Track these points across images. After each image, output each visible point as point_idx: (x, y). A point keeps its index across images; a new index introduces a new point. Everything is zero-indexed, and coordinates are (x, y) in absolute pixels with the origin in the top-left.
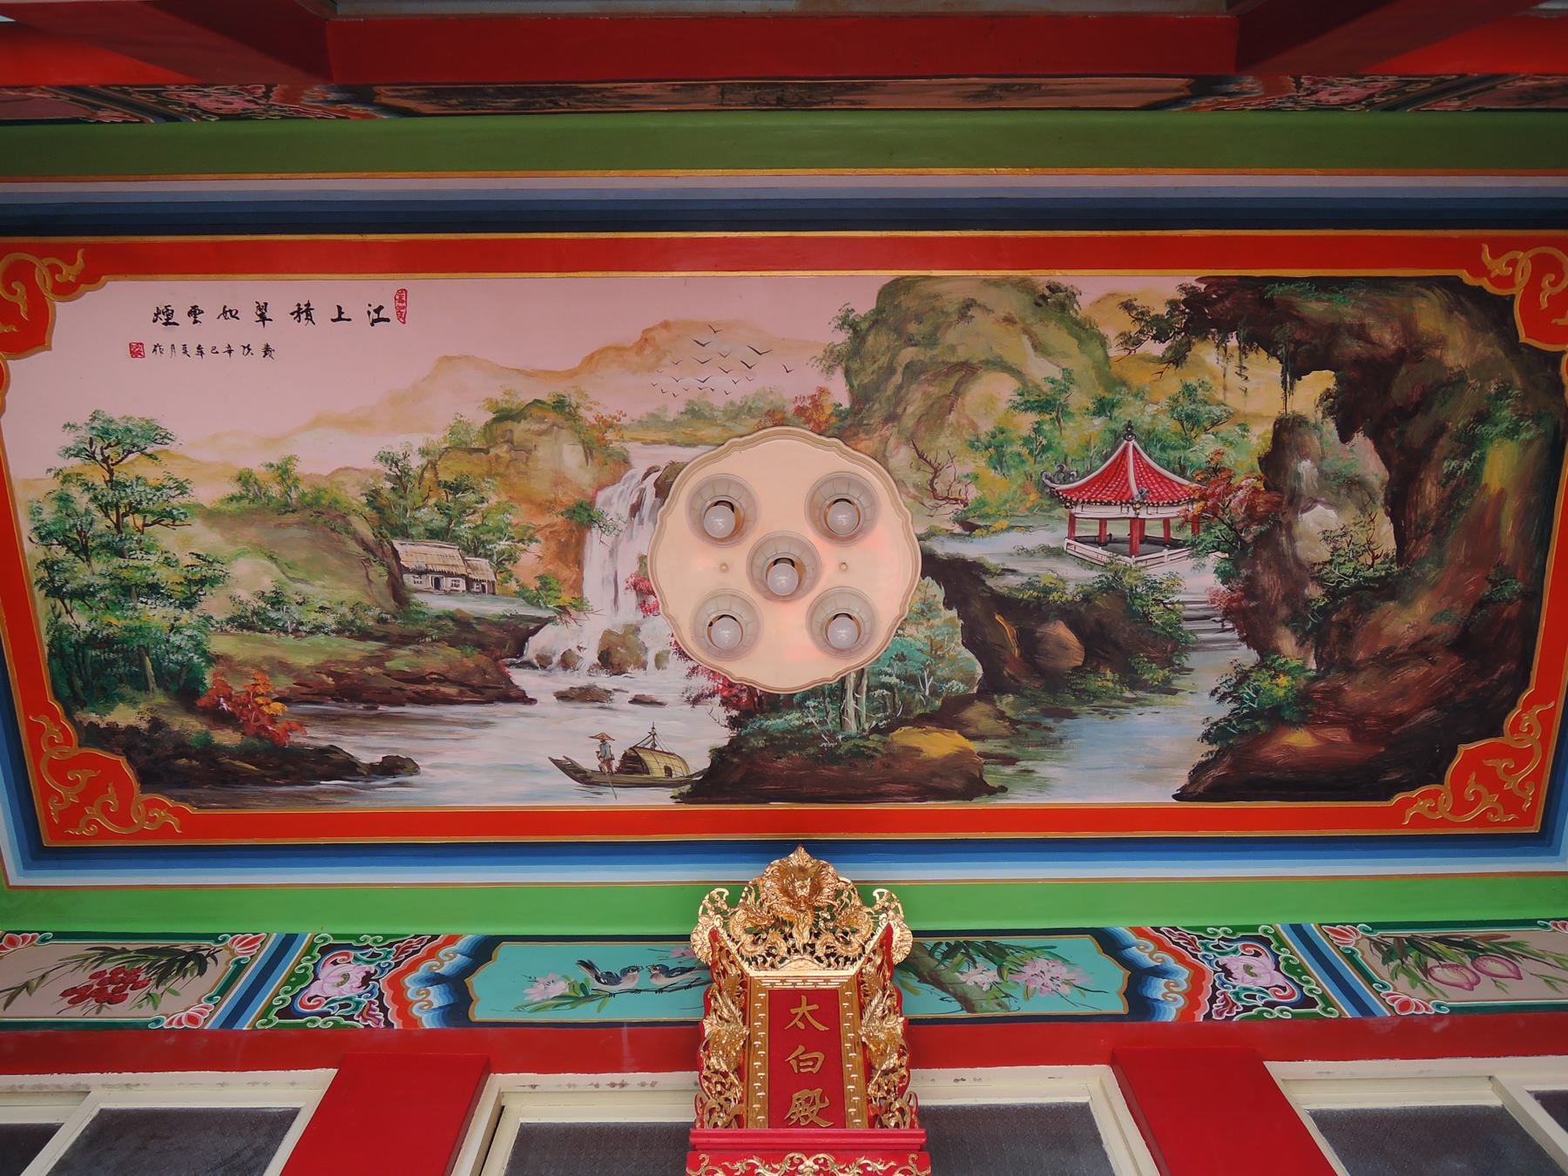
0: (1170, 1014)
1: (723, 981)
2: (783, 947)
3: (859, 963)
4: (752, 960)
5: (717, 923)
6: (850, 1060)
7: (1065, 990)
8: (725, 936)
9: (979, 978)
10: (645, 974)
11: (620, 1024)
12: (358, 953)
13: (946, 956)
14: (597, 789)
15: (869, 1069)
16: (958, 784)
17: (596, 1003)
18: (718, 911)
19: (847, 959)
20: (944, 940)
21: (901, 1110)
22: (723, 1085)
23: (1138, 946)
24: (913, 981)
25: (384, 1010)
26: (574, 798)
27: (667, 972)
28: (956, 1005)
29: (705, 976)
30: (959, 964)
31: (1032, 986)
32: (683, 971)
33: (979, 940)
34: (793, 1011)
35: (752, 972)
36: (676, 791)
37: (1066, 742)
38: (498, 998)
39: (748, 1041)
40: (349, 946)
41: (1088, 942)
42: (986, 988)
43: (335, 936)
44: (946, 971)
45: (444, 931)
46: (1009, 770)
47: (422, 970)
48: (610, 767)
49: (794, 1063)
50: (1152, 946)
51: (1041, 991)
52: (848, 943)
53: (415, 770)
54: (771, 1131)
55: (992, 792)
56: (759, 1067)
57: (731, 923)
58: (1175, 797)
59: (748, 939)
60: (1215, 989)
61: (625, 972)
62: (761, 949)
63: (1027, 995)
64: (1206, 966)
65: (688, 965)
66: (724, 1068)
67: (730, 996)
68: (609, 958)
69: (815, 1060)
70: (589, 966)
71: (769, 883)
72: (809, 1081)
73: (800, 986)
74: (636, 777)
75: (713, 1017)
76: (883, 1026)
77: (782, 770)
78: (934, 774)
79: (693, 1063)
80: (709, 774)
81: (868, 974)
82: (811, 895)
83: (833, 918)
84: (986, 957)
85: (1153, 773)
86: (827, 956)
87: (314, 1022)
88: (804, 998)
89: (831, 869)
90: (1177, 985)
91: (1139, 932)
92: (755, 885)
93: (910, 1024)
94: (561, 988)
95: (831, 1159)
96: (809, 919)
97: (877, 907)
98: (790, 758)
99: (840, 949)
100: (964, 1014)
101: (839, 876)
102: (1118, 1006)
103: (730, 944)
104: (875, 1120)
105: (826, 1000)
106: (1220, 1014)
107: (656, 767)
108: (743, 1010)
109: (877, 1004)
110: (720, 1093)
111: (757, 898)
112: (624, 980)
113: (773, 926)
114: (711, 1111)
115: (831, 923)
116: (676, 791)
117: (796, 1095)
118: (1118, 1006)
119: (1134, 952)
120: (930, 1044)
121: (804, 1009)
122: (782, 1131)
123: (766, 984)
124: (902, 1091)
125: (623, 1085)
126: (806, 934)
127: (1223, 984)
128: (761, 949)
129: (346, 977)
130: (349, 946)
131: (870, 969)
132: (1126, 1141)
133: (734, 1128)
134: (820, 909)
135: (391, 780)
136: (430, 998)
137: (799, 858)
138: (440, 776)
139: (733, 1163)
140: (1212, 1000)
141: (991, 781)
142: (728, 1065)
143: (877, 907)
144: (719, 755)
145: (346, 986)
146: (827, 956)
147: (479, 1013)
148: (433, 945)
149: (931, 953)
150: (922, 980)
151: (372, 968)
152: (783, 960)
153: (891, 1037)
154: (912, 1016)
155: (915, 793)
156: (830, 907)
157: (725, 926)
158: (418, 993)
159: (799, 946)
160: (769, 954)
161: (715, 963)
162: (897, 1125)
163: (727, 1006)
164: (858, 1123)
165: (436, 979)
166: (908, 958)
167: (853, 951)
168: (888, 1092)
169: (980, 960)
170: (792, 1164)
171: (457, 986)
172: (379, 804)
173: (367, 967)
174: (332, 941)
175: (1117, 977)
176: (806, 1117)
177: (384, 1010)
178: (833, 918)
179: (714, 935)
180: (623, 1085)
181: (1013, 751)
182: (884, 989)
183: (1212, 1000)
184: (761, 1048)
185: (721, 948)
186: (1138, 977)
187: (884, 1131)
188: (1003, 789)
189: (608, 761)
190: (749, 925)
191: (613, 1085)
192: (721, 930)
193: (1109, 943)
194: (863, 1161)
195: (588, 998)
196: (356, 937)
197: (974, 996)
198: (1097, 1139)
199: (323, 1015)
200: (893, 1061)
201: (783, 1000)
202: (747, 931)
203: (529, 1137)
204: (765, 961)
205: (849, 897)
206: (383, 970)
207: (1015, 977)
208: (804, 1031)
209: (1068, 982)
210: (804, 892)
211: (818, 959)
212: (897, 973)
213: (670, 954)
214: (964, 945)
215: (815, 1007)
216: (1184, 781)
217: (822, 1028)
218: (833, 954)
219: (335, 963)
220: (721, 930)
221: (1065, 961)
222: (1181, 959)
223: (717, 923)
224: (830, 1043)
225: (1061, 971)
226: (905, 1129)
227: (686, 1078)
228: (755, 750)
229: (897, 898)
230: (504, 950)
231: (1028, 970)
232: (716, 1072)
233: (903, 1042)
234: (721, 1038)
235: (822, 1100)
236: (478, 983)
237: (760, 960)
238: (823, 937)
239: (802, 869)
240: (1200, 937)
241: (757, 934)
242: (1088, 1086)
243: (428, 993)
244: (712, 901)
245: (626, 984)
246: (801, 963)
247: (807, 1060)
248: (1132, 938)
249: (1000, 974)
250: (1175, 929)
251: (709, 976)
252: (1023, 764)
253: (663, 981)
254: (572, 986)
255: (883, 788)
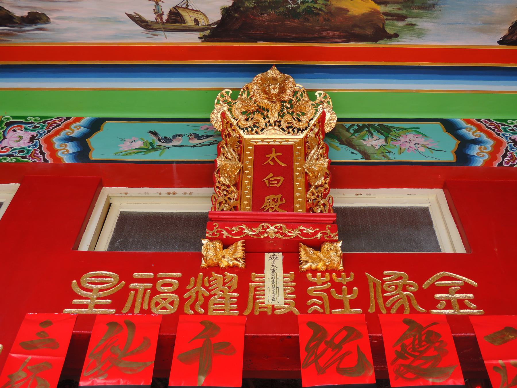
0: (479, 163)
1: (228, 139)
2: (263, 123)
3: (306, 132)
4: (245, 129)
5: (225, 109)
6: (298, 181)
7: (422, 150)
8: (230, 116)
9: (374, 143)
10: (186, 138)
11: (172, 162)
12: (27, 126)
13: (356, 131)
14: (155, 33)
15: (308, 186)
16: (369, 32)
17: (158, 152)
18: (225, 102)
19: (299, 130)
20: (356, 123)
21: (324, 205)
22: (227, 191)
23: (466, 129)
24: (336, 143)
25: (43, 154)
26: (141, 38)
27: (198, 137)
28: (360, 156)
29: (219, 139)
30: (363, 136)
31: (403, 147)
32: (207, 137)
33: (376, 124)
34: (267, 156)
35: (245, 136)
36: (201, 34)
37: (436, 7)
38: (104, 148)
39: (242, 171)
40: (22, 123)
41: (438, 126)
42: (377, 148)
43: (14, 117)
44: (356, 139)
45: (74, 115)
46: (401, 24)
47: (63, 134)
48: (161, 19)
49: (267, 182)
50: (474, 129)
51: (408, 150)
52: (300, 121)
53: (47, 20)
54: (253, 213)
55: (390, 37)
56: (247, 183)
57: (233, 109)
58: (499, 42)
59: (242, 118)
60: (507, 151)
61: (174, 137)
62: (250, 123)
63: (400, 152)
64: (504, 139)
65: (209, 134)
66: (228, 183)
67: (232, 147)
68: (165, 130)
69: (279, 181)
70: (155, 134)
71: (255, 87)
72: (275, 191)
73: (272, 143)
74: (177, 26)
75: (222, 158)
76: (318, 163)
77: (264, 21)
78: (355, 26)
79: (210, 182)
80: (221, 24)
81: (311, 137)
82: (279, 93)
83: (292, 107)
84: (379, 132)
85: (487, 27)
86: (288, 128)
87: (5, 159)
88: (274, 150)
89: (291, 80)
90: (486, 149)
91: (468, 121)
92: (247, 88)
93: (331, 164)
94: (139, 144)
95: (284, 227)
96: (278, 107)
97: (317, 101)
98: (269, 14)
99: (295, 124)
100: (364, 160)
101: (296, 85)
102: (451, 158)
103: (233, 120)
104: (310, 209)
105: (286, 151)
106: (508, 163)
107: (189, 19)
108: (239, 155)
109: (315, 152)
110: (225, 195)
111: (248, 95)
112: (174, 140)
113: (257, 111)
114: (220, 203)
115: (290, 108)
116: (201, 34)
117: (267, 198)
118: (451, 158)
119: (464, 131)
120: (341, 175)
121: (274, 155)
122: (258, 213)
123: (253, 142)
124: (325, 196)
125: (174, 194)
126: (276, 115)
127: (512, 148)
128: (250, 123)
129: (21, 138)
130: (22, 123)
131: (312, 134)
132: (440, 207)
133: (233, 211)
134: (284, 101)
135: (34, 27)
136: (68, 148)
137: (273, 73)
138: (63, 24)
139: (231, 227)
140: (504, 156)
141: (389, 30)
142: (230, 181)
143: (317, 101)
144: (226, 12)
145: (21, 142)
146: (288, 128)
147: (94, 155)
148: (68, 123)
149: (348, 130)
150: (342, 143)
151: (35, 133)
152: (263, 129)
153: (321, 169)
154: (334, 160)
155: (344, 37)
156: (290, 101)
157: (230, 110)
158: (61, 146)
159: (272, 121)
160: (255, 126)
161: (224, 130)
162: (321, 212)
163: (230, 152)
164: (299, 208)
165: (70, 139)
166: (334, 129)
167: (302, 126)
168: (318, 196)
169: (376, 134)
170: (263, 228)
171: (82, 143)
172: (29, 41)
173: (32, 133)
174: (12, 120)
175: (453, 143)
176: (272, 208)
177: (43, 154)
178: (292, 107)
179: (223, 115)
180: (174, 194)
181: (404, 12)
182: (319, 144)
183: (504, 156)
184: (249, 174)
185: (228, 122)
186: (464, 143)
187: (314, 214)
188: (396, 36)
189: (160, 15)
190: (243, 110)
191: (169, 193)
192: (228, 113)
193: (450, 127)
194: (301, 228)
195: (154, 149)
196: (25, 118)
197: (370, 151)
198: (431, 224)
199: (10, 156)
200: (321, 181)
201: (262, 151)
202: (242, 113)
203: (125, 219)
204: (252, 130)
205: (302, 95)
206: (41, 134)
207: (395, 143)
208: (273, 167)
209: (424, 146)
210: (275, 91)
211: (283, 129)
212: (328, 140)
213: (201, 128)
214: (367, 126)
215: (280, 154)
216: (506, 32)
217: (283, 165)
218: (291, 127)
219: (14, 131)
220: (228, 113)
221: (424, 135)
222: (490, 135)
223: (225, 109)
224: (288, 173)
225: (421, 140)
226: (326, 213)
227: (208, 191)
228: (248, 9)
229: (330, 98)
230: (107, 125)
231: (402, 140)
232: (224, 185)
233: (327, 171)
234: (227, 168)
235: (281, 200)
236: (93, 141)
237: (250, 129)
238: (286, 118)
239: (274, 79)
240: (503, 125)
241: (247, 114)
242: (431, 199)
243: (66, 146)
244: (222, 96)
245: (175, 143)
246: (273, 131)
247: (272, 180)
248: (464, 124)
249: (386, 141)
250: (489, 120)
251: (221, 138)
252: (409, 20)
253: (196, 142)
254: (145, 143)
255: (324, 34)
